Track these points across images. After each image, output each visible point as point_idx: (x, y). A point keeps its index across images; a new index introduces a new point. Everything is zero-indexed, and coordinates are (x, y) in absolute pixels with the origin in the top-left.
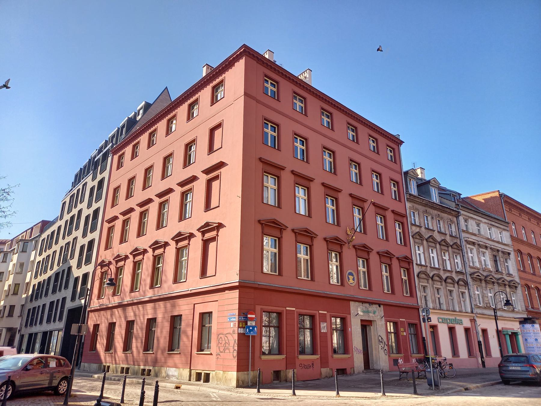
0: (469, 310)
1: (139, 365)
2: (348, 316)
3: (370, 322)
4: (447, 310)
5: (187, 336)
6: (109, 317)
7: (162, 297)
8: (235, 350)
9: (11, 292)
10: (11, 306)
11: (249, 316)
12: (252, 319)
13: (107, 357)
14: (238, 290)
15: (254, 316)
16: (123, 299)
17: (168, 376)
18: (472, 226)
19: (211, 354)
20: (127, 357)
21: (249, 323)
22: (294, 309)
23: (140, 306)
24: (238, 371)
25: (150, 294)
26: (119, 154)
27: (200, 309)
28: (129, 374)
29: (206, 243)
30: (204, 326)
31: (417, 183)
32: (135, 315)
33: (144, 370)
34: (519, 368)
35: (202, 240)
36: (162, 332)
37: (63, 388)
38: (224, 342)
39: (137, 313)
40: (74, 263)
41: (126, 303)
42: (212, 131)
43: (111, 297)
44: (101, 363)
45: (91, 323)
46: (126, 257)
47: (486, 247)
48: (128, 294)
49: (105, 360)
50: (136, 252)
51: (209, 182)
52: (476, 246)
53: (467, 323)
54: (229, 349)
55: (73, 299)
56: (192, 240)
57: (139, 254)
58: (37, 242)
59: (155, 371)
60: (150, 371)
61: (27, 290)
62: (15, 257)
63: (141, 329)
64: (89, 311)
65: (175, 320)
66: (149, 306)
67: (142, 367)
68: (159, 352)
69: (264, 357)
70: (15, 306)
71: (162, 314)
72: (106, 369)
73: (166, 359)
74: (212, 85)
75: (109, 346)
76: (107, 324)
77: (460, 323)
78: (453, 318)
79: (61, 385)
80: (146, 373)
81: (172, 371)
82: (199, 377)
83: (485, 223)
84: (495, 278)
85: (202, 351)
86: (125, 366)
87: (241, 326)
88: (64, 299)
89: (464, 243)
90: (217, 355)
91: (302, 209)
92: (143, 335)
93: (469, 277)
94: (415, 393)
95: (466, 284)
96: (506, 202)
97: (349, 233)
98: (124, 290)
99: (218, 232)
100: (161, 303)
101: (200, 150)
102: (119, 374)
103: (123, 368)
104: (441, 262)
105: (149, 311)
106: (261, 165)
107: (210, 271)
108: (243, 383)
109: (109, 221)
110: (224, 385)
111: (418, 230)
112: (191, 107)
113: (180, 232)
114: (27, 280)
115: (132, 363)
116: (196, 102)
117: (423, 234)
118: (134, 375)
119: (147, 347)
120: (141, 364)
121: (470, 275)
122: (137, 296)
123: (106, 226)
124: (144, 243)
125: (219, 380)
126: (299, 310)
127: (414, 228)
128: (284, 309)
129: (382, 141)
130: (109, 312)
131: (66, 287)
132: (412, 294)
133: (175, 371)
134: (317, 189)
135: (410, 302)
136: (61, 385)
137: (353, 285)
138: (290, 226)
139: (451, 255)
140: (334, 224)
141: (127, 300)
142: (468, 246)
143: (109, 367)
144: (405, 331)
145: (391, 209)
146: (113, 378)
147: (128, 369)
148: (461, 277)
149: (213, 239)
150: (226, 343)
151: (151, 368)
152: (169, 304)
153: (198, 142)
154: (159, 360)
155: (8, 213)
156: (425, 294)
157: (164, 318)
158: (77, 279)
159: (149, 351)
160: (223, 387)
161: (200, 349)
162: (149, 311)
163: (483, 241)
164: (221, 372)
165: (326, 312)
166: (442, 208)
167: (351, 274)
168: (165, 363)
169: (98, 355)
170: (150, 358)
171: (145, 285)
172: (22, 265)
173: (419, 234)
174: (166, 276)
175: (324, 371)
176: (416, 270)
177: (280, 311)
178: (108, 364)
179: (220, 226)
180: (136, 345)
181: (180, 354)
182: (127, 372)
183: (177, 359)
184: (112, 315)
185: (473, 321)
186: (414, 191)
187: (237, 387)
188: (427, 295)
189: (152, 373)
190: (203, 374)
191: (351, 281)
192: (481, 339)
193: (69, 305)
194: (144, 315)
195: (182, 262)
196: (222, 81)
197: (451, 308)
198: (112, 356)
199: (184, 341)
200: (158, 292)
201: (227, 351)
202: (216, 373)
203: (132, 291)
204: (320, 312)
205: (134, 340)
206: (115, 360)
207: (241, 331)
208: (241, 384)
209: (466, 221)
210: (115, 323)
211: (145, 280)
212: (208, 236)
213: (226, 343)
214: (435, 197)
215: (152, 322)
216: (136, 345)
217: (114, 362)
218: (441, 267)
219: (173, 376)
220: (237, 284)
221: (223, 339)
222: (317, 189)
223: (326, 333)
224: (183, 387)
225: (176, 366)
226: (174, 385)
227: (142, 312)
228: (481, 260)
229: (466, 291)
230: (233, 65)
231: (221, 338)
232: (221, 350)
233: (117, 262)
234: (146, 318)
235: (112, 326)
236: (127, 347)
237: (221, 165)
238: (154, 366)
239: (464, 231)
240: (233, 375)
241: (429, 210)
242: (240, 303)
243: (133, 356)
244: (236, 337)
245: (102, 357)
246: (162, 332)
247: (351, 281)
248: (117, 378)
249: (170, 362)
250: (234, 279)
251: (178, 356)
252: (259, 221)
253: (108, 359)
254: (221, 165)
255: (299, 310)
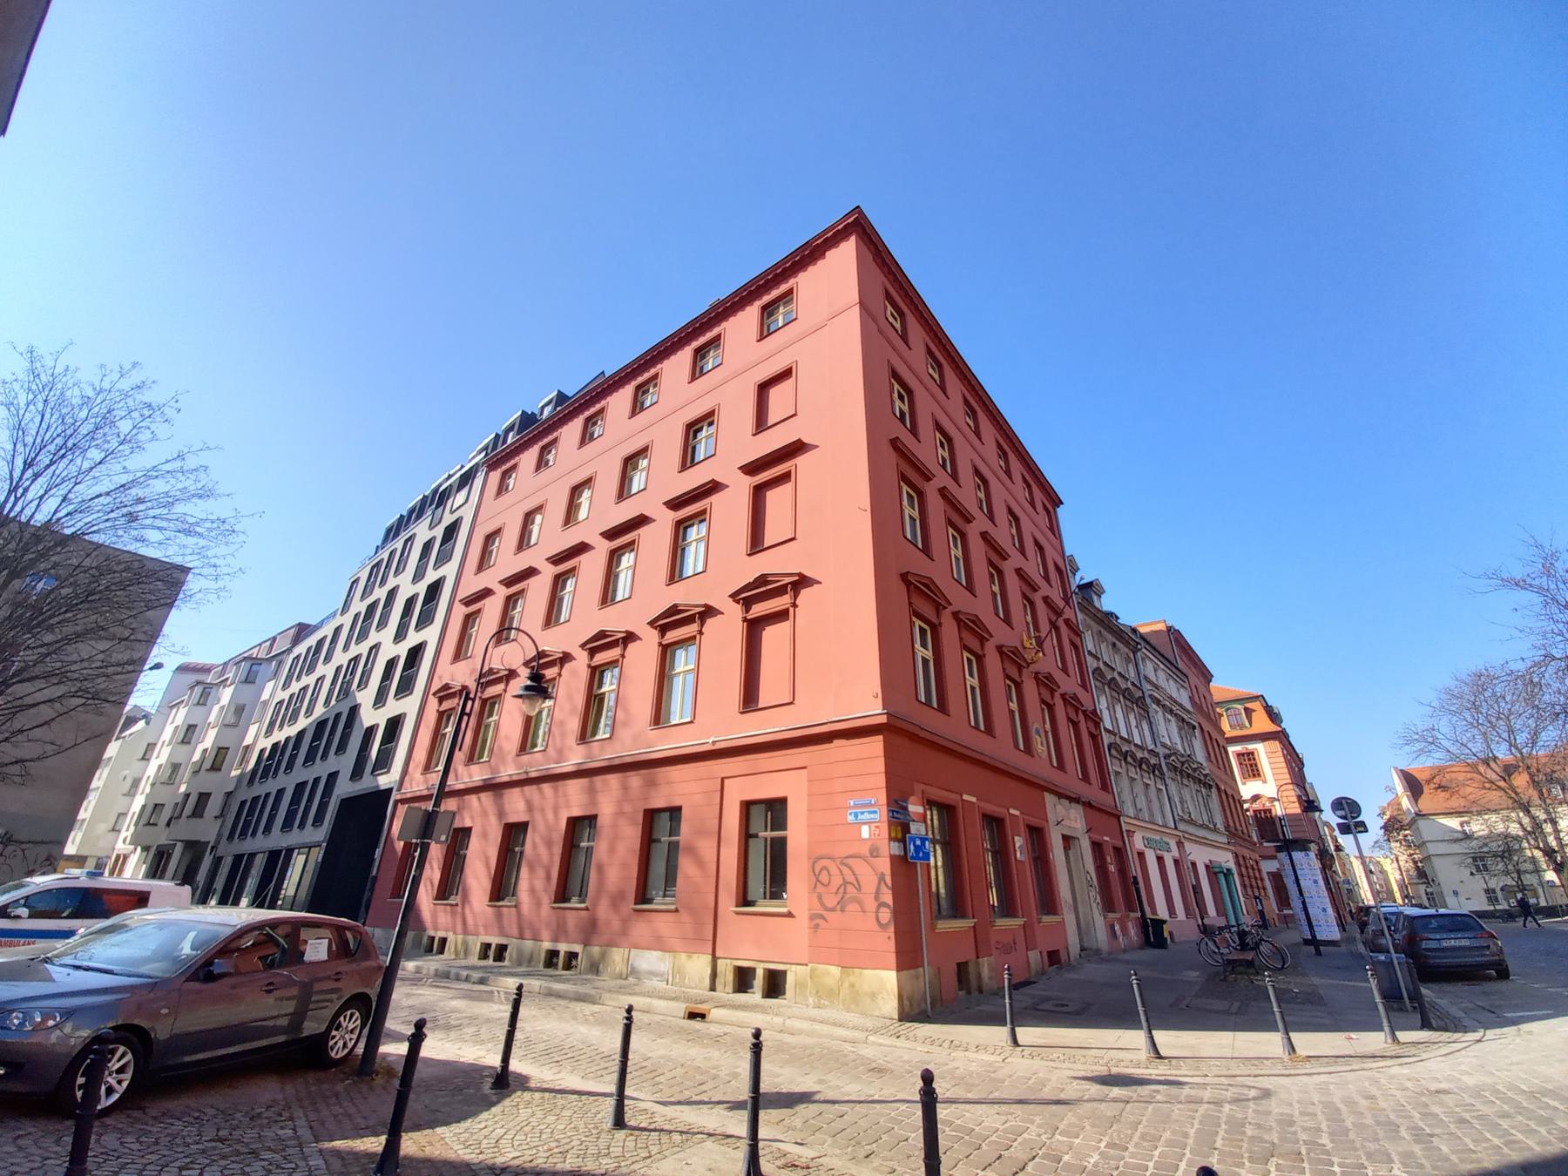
1: (536, 938)
5: (700, 863)
7: (617, 762)
9: (208, 764)
16: (495, 770)
18: (1148, 669)
19: (790, 915)
20: (499, 917)
21: (914, 827)
23: (546, 787)
24: (899, 968)
25: (575, 757)
28: (506, 963)
32: (530, 808)
33: (553, 954)
35: (745, 620)
36: (615, 854)
37: (346, 1039)
38: (837, 881)
41: (506, 779)
42: (764, 388)
51: (759, 492)
53: (1175, 853)
54: (859, 902)
55: (357, 773)
58: (280, 663)
60: (572, 956)
63: (549, 844)
66: (574, 787)
67: (547, 945)
71: (613, 805)
73: (625, 923)
77: (1169, 851)
81: (648, 960)
82: (743, 979)
86: (495, 940)
88: (333, 776)
94: (1426, 1025)
96: (1177, 640)
97: (1027, 644)
98: (500, 748)
100: (613, 780)
102: (474, 960)
105: (574, 800)
109: (468, 602)
112: (700, 353)
113: (675, 606)
114: (248, 740)
115: (515, 932)
118: (520, 965)
120: (545, 934)
122: (536, 763)
123: (460, 611)
125: (827, 995)
131: (342, 748)
132: (1105, 786)
141: (508, 772)
143: (444, 941)
146: (464, 973)
147: (502, 949)
150: (845, 883)
151: (577, 948)
152: (635, 780)
155: (226, 570)
157: (620, 813)
158: (370, 731)
164: (835, 971)
168: (624, 932)
170: (572, 919)
171: (563, 735)
172: (239, 710)
174: (626, 710)
175: (1034, 956)
176: (1106, 739)
179: (802, 582)
180: (533, 885)
185: (1180, 844)
190: (760, 973)
193: (345, 788)
198: (453, 914)
201: (853, 907)
202: (813, 971)
205: (524, 872)
208: (914, 1011)
211: (562, 723)
213: (845, 883)
216: (533, 885)
219: (652, 974)
220: (883, 719)
224: (715, 1014)
225: (659, 944)
226: (681, 1008)
232: (829, 904)
234: (564, 815)
236: (501, 888)
237: (797, 448)
238: (586, 944)
240: (885, 982)
243: (519, 914)
244: (885, 866)
246: (612, 850)
248: (476, 975)
249: (640, 929)
252: (904, 577)
254: (797, 448)
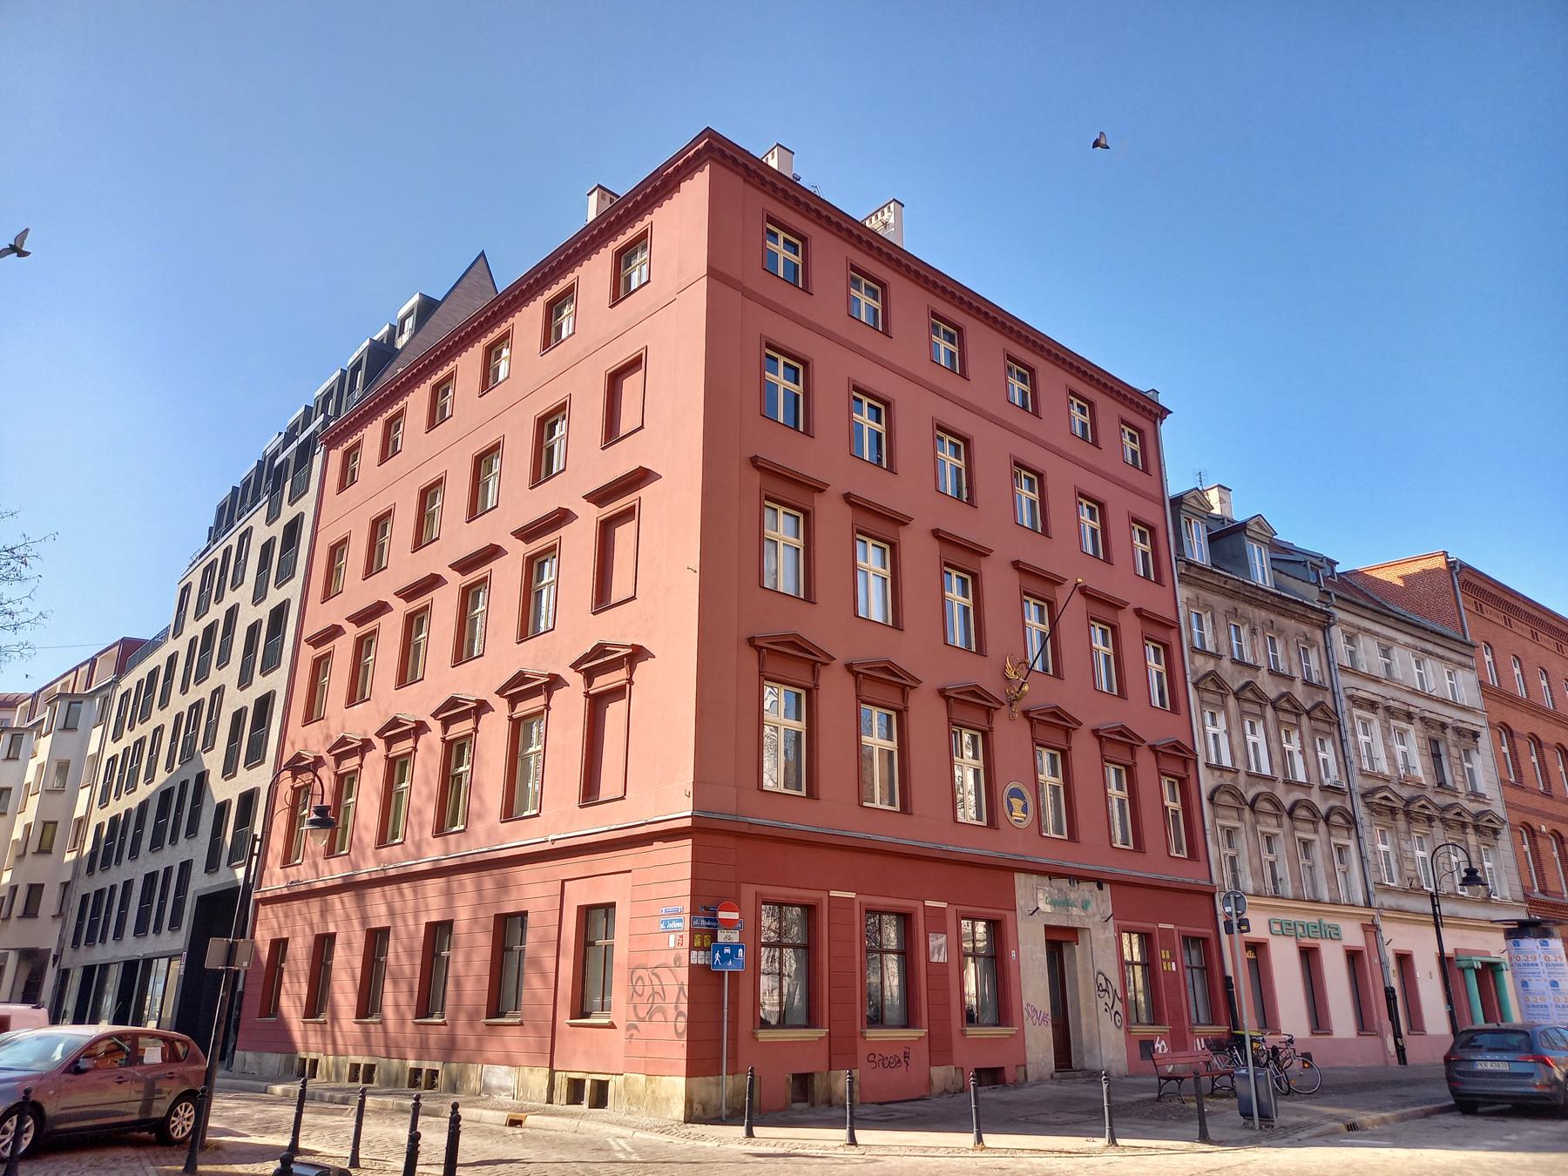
0: (1360, 898)
1: (403, 1058)
2: (1009, 914)
3: (1073, 933)
4: (1296, 899)
5: (543, 975)
6: (316, 918)
7: (469, 860)
8: (680, 1014)
9: (33, 846)
10: (31, 887)
11: (722, 915)
12: (729, 925)
13: (311, 1034)
14: (689, 841)
15: (735, 916)
16: (355, 866)
17: (486, 1088)
18: (1369, 655)
19: (612, 1026)
20: (367, 1035)
21: (722, 936)
22: (853, 895)
23: (406, 887)
24: (690, 1073)
25: (435, 852)
26: (346, 445)
27: (580, 895)
28: (375, 1084)
29: (597, 705)
30: (593, 944)
31: (1208, 530)
32: (392, 913)
33: (416, 1072)
34: (1503, 1067)
35: (587, 695)
36: (470, 963)
37: (182, 1124)
38: (648, 991)
39: (397, 905)
40: (213, 761)
41: (365, 877)
42: (615, 379)
43: (320, 861)
44: (294, 1051)
45: (263, 937)
46: (367, 745)
47: (1409, 717)
48: (370, 851)
49: (306, 1043)
50: (394, 731)
51: (606, 528)
52: (1381, 711)
53: (1353, 936)
54: (664, 1012)
55: (212, 865)
56: (558, 694)
57: (403, 736)
58: (106, 701)
59: (449, 1074)
60: (434, 1073)
61: (78, 840)
62: (44, 745)
63: (410, 953)
64: (257, 902)
65: (508, 928)
66: (433, 886)
67: (412, 1064)
68: (462, 1021)
69: (764, 1035)
70: (42, 886)
71: (468, 909)
72: (306, 1070)
73: (480, 1040)
74: (614, 246)
75: (317, 1003)
76: (311, 940)
77: (1334, 935)
78: (1314, 920)
79: (177, 1115)
80: (423, 1080)
81: (499, 1075)
82: (575, 1091)
83: (1406, 645)
84: (1436, 807)
85: (587, 1015)
86: (363, 1061)
87: (697, 943)
88: (186, 866)
89: (1345, 704)
90: (628, 1028)
91: (874, 605)
92: (413, 972)
93: (1358, 801)
94: (1204, 1138)
95: (1351, 822)
96: (1466, 585)
97: (1011, 675)
98: (360, 839)
99: (631, 672)
100: (468, 879)
101: (580, 435)
102: (345, 1083)
103: (355, 1067)
104: (1277, 758)
105: (431, 902)
106: (756, 478)
107: (609, 784)
108: (704, 1109)
109: (317, 641)
110: (649, 1115)
111: (1210, 665)
112: (554, 309)
113: (521, 673)
114: (80, 812)
115: (382, 1051)
116: (568, 294)
117: (1226, 677)
118: (388, 1085)
119: (427, 1005)
120: (410, 1053)
121: (1363, 796)
122: (396, 858)
123: (308, 653)
124: (417, 703)
125: (634, 1099)
126: (866, 899)
127: (1199, 660)
128: (823, 895)
129: (1108, 409)
130: (315, 904)
131: (192, 831)
132: (1195, 851)
133: (508, 1074)
134: (919, 548)
135: (1188, 875)
136: (177, 1115)
137: (1024, 825)
138: (841, 656)
139: (1307, 739)
140: (968, 649)
141: (368, 868)
142: (1357, 712)
143: (315, 1062)
144: (1173, 958)
145: (1134, 604)
146: (328, 1094)
147: (370, 1069)
148: (1335, 802)
149: (618, 693)
150: (654, 993)
151: (438, 1066)
152: (488, 880)
153: (575, 411)
154: (460, 1043)
155: (24, 617)
156: (1231, 853)
157: (475, 920)
158: (222, 808)
159: (431, 1015)
160: (645, 1120)
161: (581, 1010)
162: (431, 902)
163: (1399, 699)
164: (642, 1078)
165: (944, 905)
166: (1280, 604)
167: (1016, 793)
168: (480, 1050)
169: (283, 1029)
170: (434, 1037)
171: (421, 825)
172: (63, 768)
173: (1214, 676)
174: (480, 798)
175: (940, 1074)
176: (1207, 781)
177: (811, 902)
178: (313, 1056)
179: (638, 654)
180: (396, 999)
181: (521, 1024)
182: (368, 1078)
183: (512, 1039)
184: (323, 913)
185: (1371, 929)
186: (1199, 552)
187: (686, 1122)
188: (1237, 856)
189: (441, 1080)
190: (588, 1083)
191: (1018, 814)
192: (1395, 983)
193: (200, 883)
194: (416, 913)
195: (527, 760)
196: (643, 236)
197: (1307, 892)
198: (323, 1032)
199: (535, 987)
200: (458, 845)
201: (658, 1017)
202: (626, 1080)
203: (382, 841)
204: (928, 903)
205: (388, 986)
206: (334, 1043)
207: (699, 958)
208: (698, 1113)
209: (1350, 639)
210: (332, 937)
211: (419, 812)
212: (602, 683)
213: (654, 993)
214: (1261, 572)
215: (439, 932)
216: (396, 999)
217: (330, 1047)
218: (1279, 774)
219: (502, 1089)
220: (688, 823)
221: (647, 982)
222: (919, 548)
223: (944, 966)
224: (530, 1120)
225: (509, 1061)
226: (503, 1116)
227: (411, 904)
228: (1394, 754)
229: (1352, 844)
230: (676, 188)
231: (640, 978)
232: (642, 1015)
233: (339, 759)
234: (424, 920)
235: (324, 945)
236: (368, 1004)
237: (641, 477)
238: (446, 1061)
239: (1344, 669)
240: (675, 1086)
241: (1243, 608)
242: (695, 879)
243: (385, 1031)
244: (684, 975)
245: (297, 1035)
246: (468, 962)
247: (1018, 814)
248: (339, 1095)
249: (493, 1048)
250: (679, 808)
251: (516, 1031)
252: (751, 641)
253: (314, 1040)
254: (641, 477)
255: (866, 899)
